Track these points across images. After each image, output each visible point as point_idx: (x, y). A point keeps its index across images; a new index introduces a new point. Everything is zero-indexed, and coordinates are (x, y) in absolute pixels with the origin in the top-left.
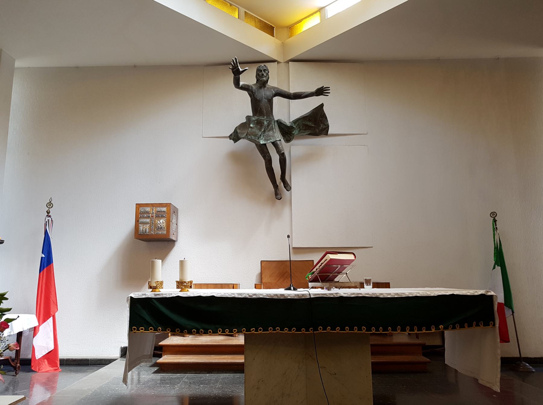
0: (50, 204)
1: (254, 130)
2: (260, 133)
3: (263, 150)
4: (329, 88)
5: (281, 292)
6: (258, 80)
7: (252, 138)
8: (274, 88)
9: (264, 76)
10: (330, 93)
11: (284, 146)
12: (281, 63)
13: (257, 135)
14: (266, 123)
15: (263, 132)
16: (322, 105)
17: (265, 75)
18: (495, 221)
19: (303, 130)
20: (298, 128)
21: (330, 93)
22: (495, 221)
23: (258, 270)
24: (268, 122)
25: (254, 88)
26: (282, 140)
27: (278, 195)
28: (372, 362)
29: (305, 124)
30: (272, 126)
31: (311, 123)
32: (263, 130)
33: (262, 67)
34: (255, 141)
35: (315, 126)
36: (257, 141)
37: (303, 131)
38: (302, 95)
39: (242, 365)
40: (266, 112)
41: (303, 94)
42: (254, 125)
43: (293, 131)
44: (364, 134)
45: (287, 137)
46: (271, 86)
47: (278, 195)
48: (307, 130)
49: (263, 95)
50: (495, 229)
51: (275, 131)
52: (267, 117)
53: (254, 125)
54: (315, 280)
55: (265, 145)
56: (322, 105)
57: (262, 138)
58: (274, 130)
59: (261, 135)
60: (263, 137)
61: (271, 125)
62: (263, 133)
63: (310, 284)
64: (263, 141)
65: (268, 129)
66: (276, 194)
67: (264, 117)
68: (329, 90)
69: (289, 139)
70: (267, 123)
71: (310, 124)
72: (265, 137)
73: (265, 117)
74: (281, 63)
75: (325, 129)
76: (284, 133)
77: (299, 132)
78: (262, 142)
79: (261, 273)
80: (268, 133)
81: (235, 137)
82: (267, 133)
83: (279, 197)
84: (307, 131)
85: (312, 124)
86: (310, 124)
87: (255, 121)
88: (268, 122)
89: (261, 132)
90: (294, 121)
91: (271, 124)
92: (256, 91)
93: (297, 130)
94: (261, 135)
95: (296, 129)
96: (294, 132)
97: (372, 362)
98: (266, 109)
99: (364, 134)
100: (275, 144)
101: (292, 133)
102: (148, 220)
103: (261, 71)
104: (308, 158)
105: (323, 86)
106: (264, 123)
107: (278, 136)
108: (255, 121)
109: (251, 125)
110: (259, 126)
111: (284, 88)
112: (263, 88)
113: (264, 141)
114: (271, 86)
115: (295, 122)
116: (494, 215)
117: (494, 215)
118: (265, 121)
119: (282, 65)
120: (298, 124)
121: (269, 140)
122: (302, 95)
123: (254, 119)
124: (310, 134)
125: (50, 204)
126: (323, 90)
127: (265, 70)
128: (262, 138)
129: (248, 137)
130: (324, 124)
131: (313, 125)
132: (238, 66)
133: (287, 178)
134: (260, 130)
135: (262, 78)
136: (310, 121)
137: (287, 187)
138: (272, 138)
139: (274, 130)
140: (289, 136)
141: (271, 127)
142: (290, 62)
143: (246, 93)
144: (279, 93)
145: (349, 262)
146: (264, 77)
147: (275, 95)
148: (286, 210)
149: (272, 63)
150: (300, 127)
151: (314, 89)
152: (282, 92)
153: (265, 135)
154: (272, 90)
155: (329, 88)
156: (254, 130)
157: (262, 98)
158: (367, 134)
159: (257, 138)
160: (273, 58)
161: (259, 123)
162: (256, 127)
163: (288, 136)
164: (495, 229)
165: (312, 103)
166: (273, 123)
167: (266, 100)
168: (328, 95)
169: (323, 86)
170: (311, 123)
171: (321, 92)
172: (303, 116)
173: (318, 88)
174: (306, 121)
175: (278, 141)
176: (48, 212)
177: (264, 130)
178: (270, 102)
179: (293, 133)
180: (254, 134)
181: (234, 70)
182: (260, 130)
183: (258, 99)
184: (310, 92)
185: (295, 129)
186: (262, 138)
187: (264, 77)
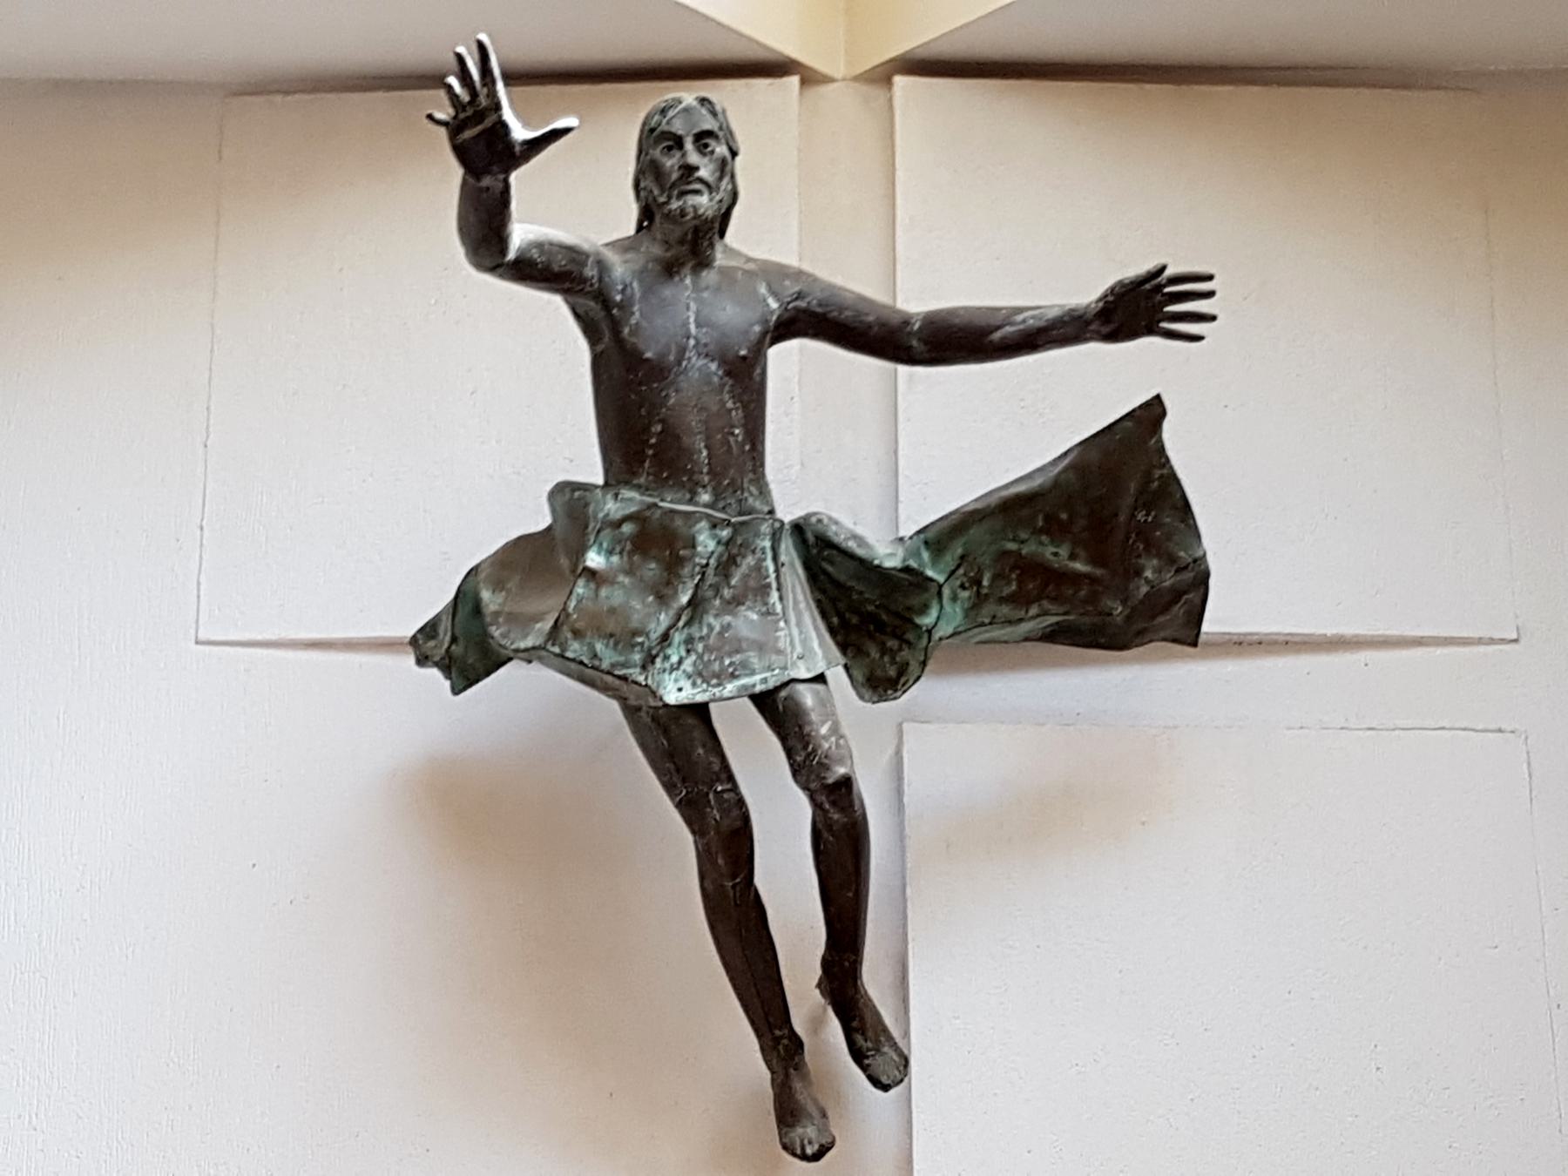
1: (612, 596)
2: (664, 619)
4: (1210, 278)
6: (648, 214)
7: (595, 656)
8: (774, 273)
9: (701, 180)
10: (1213, 318)
12: (835, 85)
13: (635, 633)
14: (707, 543)
15: (683, 609)
16: (1151, 414)
17: (703, 173)
19: (1003, 600)
20: (963, 587)
21: (1213, 318)
24: (725, 533)
26: (838, 677)
29: (1018, 554)
30: (759, 568)
31: (1064, 552)
32: (685, 599)
33: (687, 110)
34: (624, 678)
35: (1099, 572)
36: (641, 679)
37: (1005, 610)
40: (709, 456)
41: (998, 328)
42: (615, 559)
43: (924, 609)
44: (1492, 641)
45: (874, 653)
46: (752, 254)
48: (1038, 599)
49: (686, 324)
51: (779, 608)
52: (717, 496)
56: (1151, 414)
57: (674, 659)
58: (775, 596)
59: (665, 637)
60: (688, 651)
61: (750, 560)
62: (688, 624)
64: (686, 684)
65: (727, 593)
66: (788, 1112)
67: (694, 493)
68: (1210, 294)
69: (892, 672)
70: (719, 543)
71: (1056, 554)
73: (705, 497)
74: (831, 80)
75: (1177, 594)
76: (855, 620)
77: (967, 613)
78: (676, 691)
80: (728, 618)
82: (714, 621)
83: (808, 1132)
84: (1034, 611)
85: (1073, 557)
86: (1056, 554)
88: (725, 533)
89: (672, 612)
90: (930, 534)
91: (748, 548)
92: (638, 295)
93: (954, 598)
94: (665, 637)
95: (946, 592)
96: (934, 613)
98: (708, 438)
99: (1492, 641)
100: (766, 702)
101: (918, 627)
105: (1163, 268)
108: (627, 528)
110: (653, 565)
112: (687, 270)
113: (694, 685)
114: (749, 260)
115: (939, 537)
118: (703, 524)
120: (960, 551)
121: (733, 676)
122: (997, 336)
123: (612, 507)
124: (1052, 636)
126: (1159, 297)
127: (710, 134)
128: (680, 662)
129: (564, 650)
130: (1172, 559)
131: (1079, 566)
132: (497, 107)
134: (663, 599)
135: (683, 194)
136: (1054, 529)
138: (754, 659)
139: (775, 596)
140: (892, 643)
141: (746, 577)
142: (900, 81)
143: (553, 308)
144: (813, 314)
146: (697, 192)
149: (761, 84)
150: (978, 583)
151: (1086, 293)
152: (841, 309)
154: (763, 290)
155: (1210, 278)
156: (612, 596)
157: (682, 350)
158: (1516, 641)
159: (637, 657)
160: (750, 39)
162: (629, 572)
163: (884, 651)
166: (767, 544)
167: (713, 366)
168: (1197, 338)
169: (1163, 268)
170: (1064, 552)
172: (1005, 493)
173: (1120, 283)
174: (1023, 535)
175: (801, 687)
180: (611, 626)
181: (468, 134)
182: (663, 599)
183: (648, 355)
184: (1053, 314)
185: (940, 594)
186: (680, 662)
187: (697, 186)
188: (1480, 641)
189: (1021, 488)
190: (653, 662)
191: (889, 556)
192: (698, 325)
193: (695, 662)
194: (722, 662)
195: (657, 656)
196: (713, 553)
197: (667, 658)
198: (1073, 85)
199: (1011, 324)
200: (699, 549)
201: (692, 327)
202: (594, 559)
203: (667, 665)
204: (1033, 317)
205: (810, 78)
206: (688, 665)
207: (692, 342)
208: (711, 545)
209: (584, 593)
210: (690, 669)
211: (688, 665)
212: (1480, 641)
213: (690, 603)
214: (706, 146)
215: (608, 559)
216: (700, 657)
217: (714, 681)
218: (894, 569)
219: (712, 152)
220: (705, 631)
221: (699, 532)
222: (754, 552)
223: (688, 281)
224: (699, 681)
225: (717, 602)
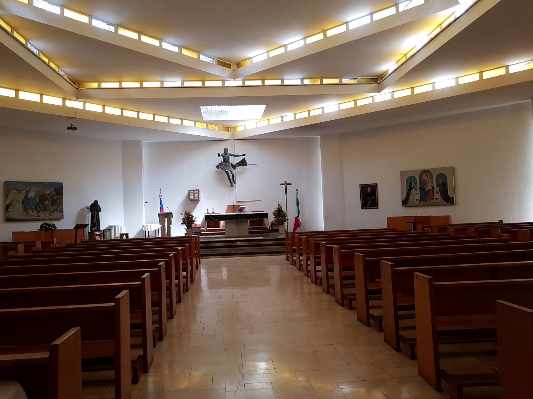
0: (160, 190)
1: (224, 167)
3: (227, 173)
5: (232, 214)
6: (225, 152)
11: (233, 171)
14: (227, 165)
16: (244, 158)
18: (297, 192)
22: (297, 192)
23: (226, 208)
25: (224, 155)
26: (233, 169)
27: (232, 185)
28: (415, 310)
39: (225, 229)
47: (232, 185)
50: (297, 194)
54: (238, 211)
56: (244, 158)
63: (238, 212)
66: (231, 185)
68: (414, 328)
78: (226, 170)
79: (227, 209)
81: (218, 167)
83: (232, 186)
97: (415, 310)
100: (230, 171)
102: (192, 195)
104: (241, 173)
107: (231, 168)
109: (223, 166)
111: (233, 153)
115: (236, 164)
116: (297, 190)
117: (297, 190)
119: (232, 141)
123: (224, 163)
125: (160, 190)
136: (241, 163)
145: (245, 207)
147: (230, 156)
148: (235, 189)
151: (242, 155)
156: (224, 167)
161: (225, 165)
164: (297, 194)
165: (242, 158)
171: (244, 155)
176: (160, 193)
178: (229, 158)
191: (234, 165)
198: (379, 300)
202: (223, 166)
209: (225, 267)
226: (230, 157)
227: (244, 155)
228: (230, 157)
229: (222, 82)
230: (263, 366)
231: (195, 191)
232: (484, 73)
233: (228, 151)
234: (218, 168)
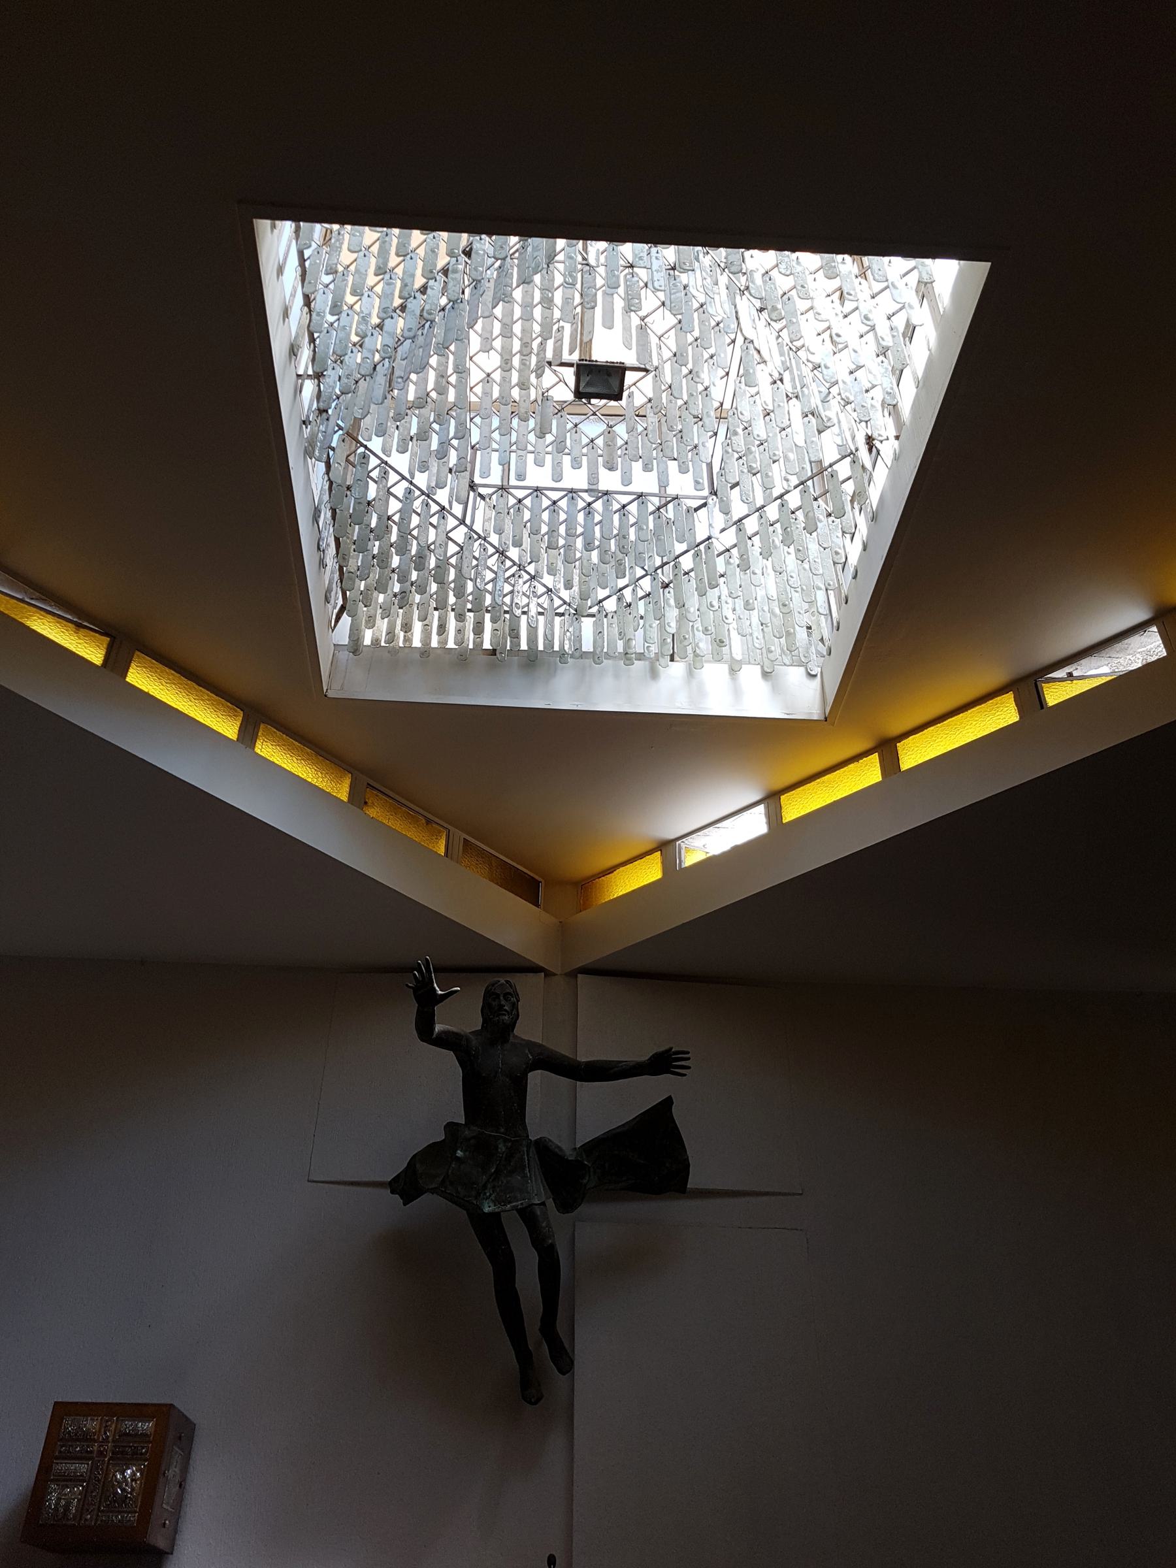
4: (688, 1053)
9: (506, 1010)
11: (556, 1221)
14: (502, 1148)
15: (492, 1174)
16: (668, 1102)
17: (506, 1008)
25: (474, 1042)
26: (550, 1203)
33: (502, 984)
36: (475, 1202)
38: (612, 1071)
42: (467, 1153)
53: (467, 1153)
55: (496, 1216)
56: (668, 1102)
57: (488, 1194)
59: (485, 1187)
60: (493, 1192)
62: (493, 1181)
72: (498, 1190)
73: (502, 1130)
80: (509, 1179)
87: (472, 1141)
95: (592, 1170)
96: (587, 1178)
99: (794, 1194)
100: (528, 1216)
102: (83, 1468)
103: (498, 996)
106: (497, 1148)
107: (537, 1192)
109: (459, 1153)
113: (495, 1206)
114: (524, 1040)
115: (592, 1147)
121: (510, 1202)
122: (612, 1071)
127: (509, 994)
128: (490, 1196)
133: (561, 1328)
137: (564, 1360)
142: (579, 975)
147: (537, 1064)
153: (498, 1187)
154: (527, 1051)
155: (688, 1053)
159: (474, 1193)
160: (534, 963)
167: (507, 1080)
168: (685, 1075)
171: (662, 1063)
173: (656, 1054)
177: (496, 1168)
179: (585, 1181)
186: (490, 1196)
187: (504, 1012)
188: (789, 1194)
189: (618, 1131)
190: (480, 1196)
191: (570, 1155)
192: (502, 1064)
193: (495, 1197)
194: (506, 1196)
195: (481, 1193)
196: (504, 1152)
197: (485, 1194)
199: (617, 1067)
200: (499, 1150)
201: (500, 1064)
203: (485, 1197)
204: (625, 1065)
205: (548, 974)
206: (493, 1197)
207: (500, 1070)
208: (504, 1149)
210: (493, 1199)
211: (493, 1197)
212: (789, 1194)
213: (494, 1171)
214: (508, 998)
215: (464, 1154)
216: (498, 1194)
217: (503, 1204)
218: (572, 1160)
219: (510, 1000)
220: (500, 1183)
221: (500, 1144)
222: (520, 1152)
223: (499, 1047)
224: (497, 1203)
225: (505, 1172)
226: (536, 1079)
227: (662, 1063)
228: (536, 1079)
229: (590, 356)
230: (510, 1144)
231: (128, 1425)
232: (403, 320)
233: (514, 1006)
234: (407, 1198)
